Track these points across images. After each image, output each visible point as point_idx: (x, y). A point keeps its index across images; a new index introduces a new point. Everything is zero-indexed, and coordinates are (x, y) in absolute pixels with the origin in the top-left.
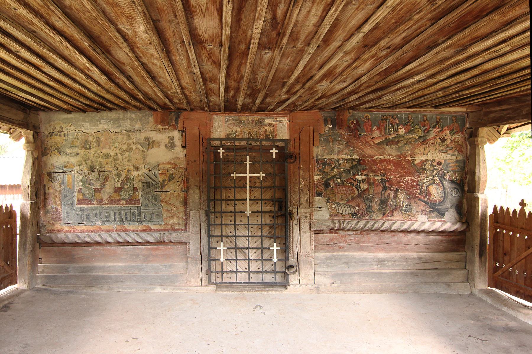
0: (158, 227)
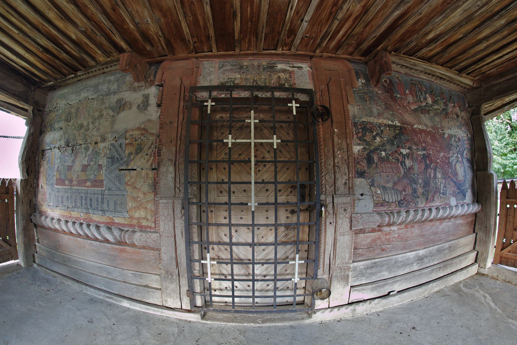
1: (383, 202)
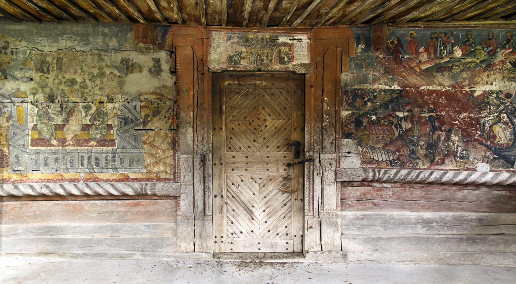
0: (138, 176)
1: (371, 160)
